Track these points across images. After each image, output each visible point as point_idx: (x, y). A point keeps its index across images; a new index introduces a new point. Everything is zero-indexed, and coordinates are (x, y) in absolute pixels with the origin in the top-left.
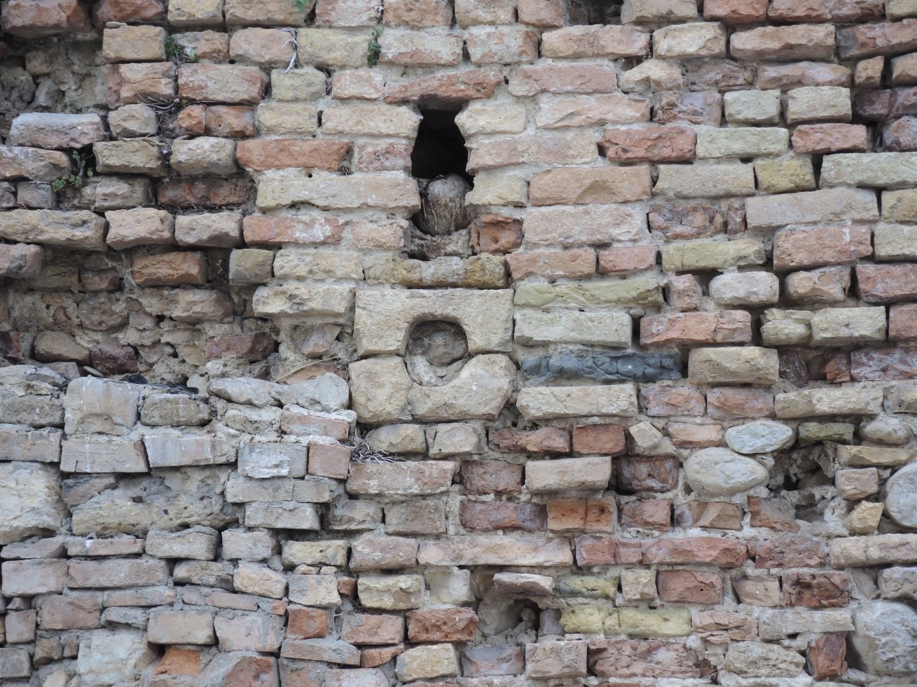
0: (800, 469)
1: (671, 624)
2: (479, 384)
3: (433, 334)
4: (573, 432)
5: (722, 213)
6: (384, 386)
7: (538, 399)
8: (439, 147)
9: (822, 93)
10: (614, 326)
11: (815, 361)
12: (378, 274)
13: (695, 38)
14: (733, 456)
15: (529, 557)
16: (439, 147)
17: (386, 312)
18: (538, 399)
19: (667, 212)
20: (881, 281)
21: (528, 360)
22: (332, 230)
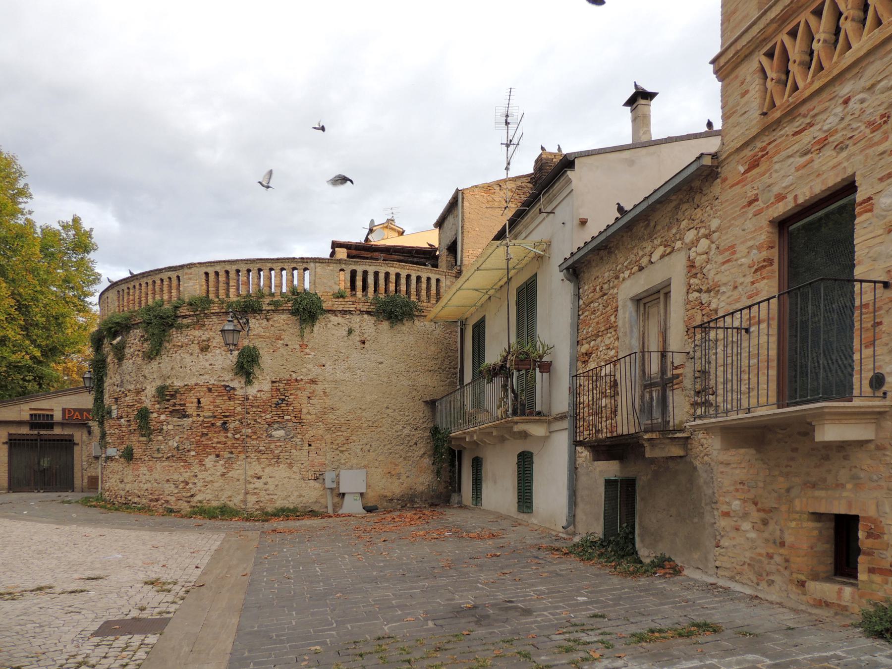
2: (201, 419)
3: (198, 415)
4: (208, 422)
5: (218, 406)
6: (195, 419)
8: (199, 402)
9: (226, 398)
11: (224, 416)
12: (159, 465)
14: (219, 423)
15: (205, 431)
16: (199, 402)
17: (195, 413)
19: (215, 406)
21: (205, 417)
22: (191, 409)
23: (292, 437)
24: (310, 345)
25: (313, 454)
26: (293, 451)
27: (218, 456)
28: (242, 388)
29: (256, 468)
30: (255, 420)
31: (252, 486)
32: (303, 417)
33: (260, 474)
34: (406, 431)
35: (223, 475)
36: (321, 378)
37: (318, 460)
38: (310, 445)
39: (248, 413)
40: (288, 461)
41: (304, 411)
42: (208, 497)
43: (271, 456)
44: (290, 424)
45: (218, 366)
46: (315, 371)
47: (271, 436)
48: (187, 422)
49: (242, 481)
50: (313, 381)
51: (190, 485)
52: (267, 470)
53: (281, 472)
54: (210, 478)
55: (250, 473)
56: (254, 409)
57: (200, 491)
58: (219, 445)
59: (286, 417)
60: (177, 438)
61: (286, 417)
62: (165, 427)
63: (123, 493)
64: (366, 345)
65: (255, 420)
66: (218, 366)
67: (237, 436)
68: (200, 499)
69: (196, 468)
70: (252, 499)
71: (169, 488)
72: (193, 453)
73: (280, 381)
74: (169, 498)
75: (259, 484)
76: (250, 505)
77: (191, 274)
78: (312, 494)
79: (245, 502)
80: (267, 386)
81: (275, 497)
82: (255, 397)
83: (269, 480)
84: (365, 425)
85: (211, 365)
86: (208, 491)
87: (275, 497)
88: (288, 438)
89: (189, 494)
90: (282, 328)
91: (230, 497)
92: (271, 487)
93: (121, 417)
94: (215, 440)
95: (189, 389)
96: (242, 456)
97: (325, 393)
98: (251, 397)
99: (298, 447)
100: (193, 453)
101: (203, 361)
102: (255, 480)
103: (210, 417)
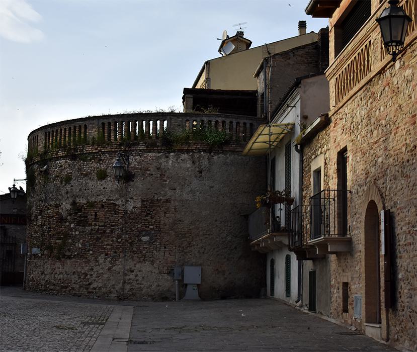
0: (112, 231)
1: (106, 239)
2: (97, 227)
5: (108, 218)
7: (100, 228)
10: (103, 224)
11: (112, 226)
12: (68, 261)
13: (107, 209)
15: (99, 236)
16: (96, 215)
18: (100, 228)
20: (115, 222)
21: (99, 226)
23: (154, 242)
24: (167, 175)
25: (167, 255)
26: (155, 252)
27: (107, 255)
28: (123, 205)
29: (130, 264)
30: (131, 229)
31: (128, 277)
32: (162, 226)
33: (133, 268)
34: (229, 238)
35: (109, 269)
36: (173, 198)
37: (171, 259)
38: (165, 248)
39: (127, 223)
40: (151, 259)
41: (162, 222)
42: (100, 285)
43: (140, 255)
44: (153, 232)
45: (108, 190)
46: (170, 193)
47: (141, 240)
48: (88, 229)
49: (121, 274)
50: (168, 201)
51: (89, 276)
52: (137, 266)
53: (146, 267)
54: (101, 271)
55: (127, 268)
56: (131, 221)
57: (95, 280)
58: (108, 247)
59: (151, 227)
60: (81, 241)
61: (151, 227)
62: (74, 233)
63: (43, 282)
64: (203, 174)
65: (131, 229)
66: (108, 190)
67: (119, 240)
68: (95, 286)
69: (92, 264)
70: (128, 287)
71: (74, 278)
72: (91, 252)
73: (147, 201)
74: (74, 286)
75: (132, 276)
76: (126, 291)
77: (94, 124)
78: (166, 282)
79: (123, 289)
80: (139, 204)
81: (142, 286)
82: (132, 213)
83: (138, 273)
84: (201, 233)
85: (104, 188)
86: (100, 281)
87: (142, 286)
88: (150, 243)
89: (88, 283)
90: (149, 162)
91: (113, 285)
92: (140, 279)
93: (44, 225)
94: (106, 243)
95: (92, 205)
96: (122, 255)
97: (175, 209)
98: (128, 212)
99: (158, 249)
100: (91, 252)
101: (99, 185)
102: (130, 273)
103: (102, 226)
